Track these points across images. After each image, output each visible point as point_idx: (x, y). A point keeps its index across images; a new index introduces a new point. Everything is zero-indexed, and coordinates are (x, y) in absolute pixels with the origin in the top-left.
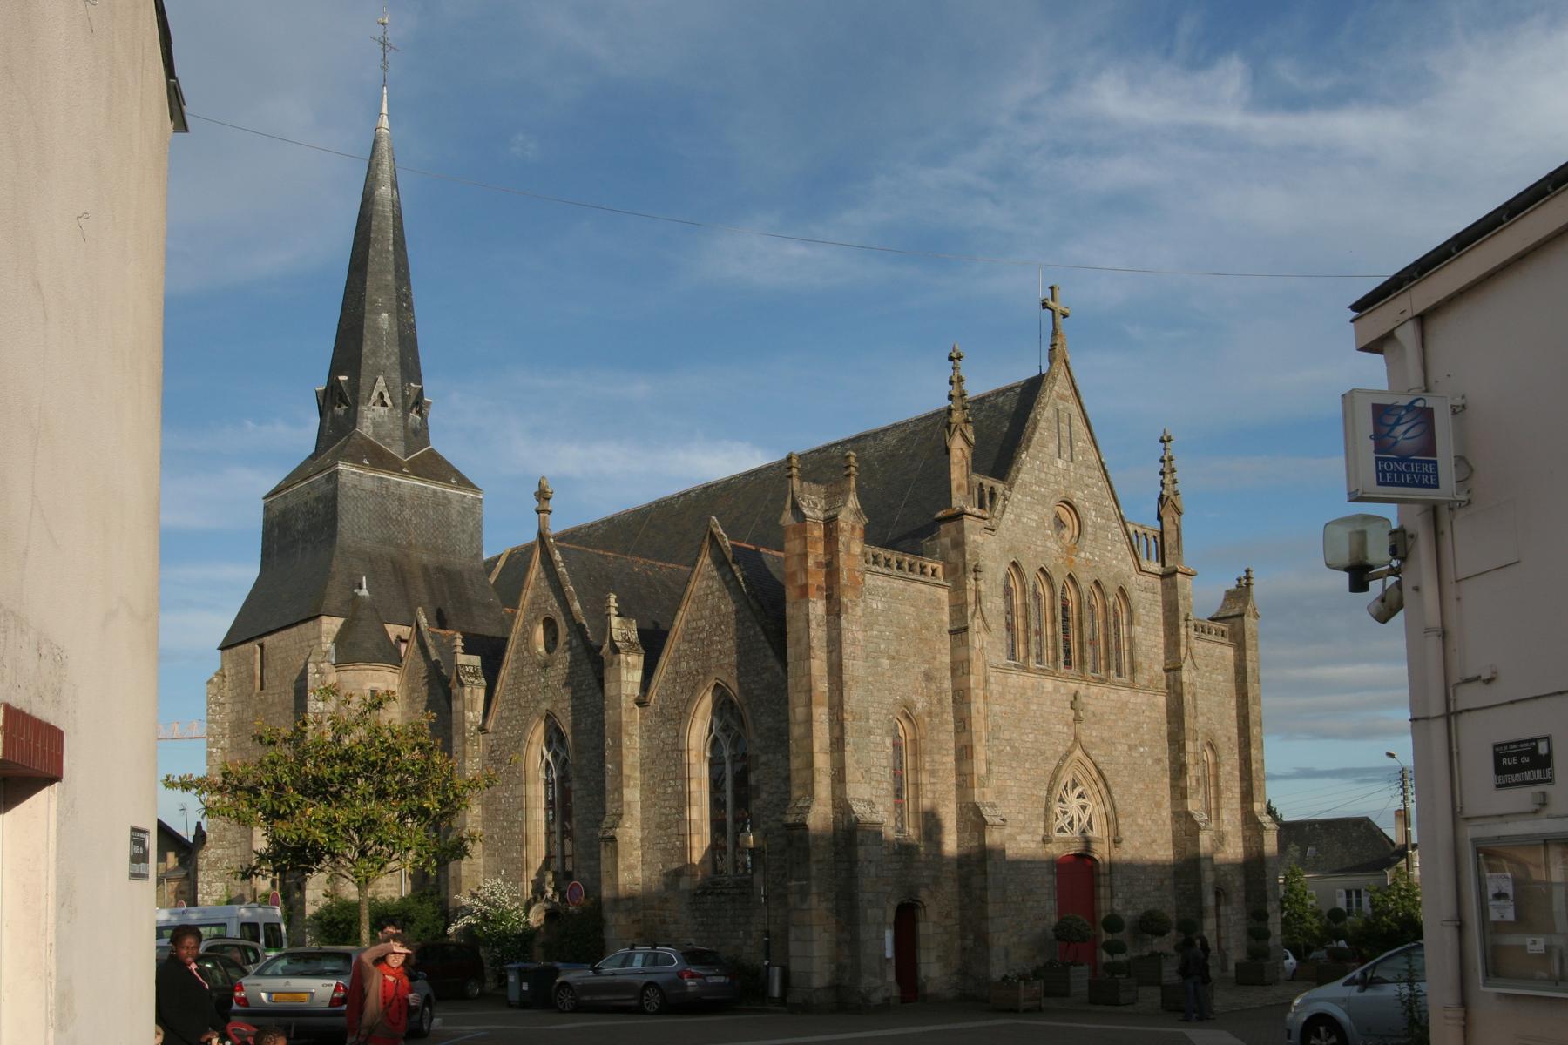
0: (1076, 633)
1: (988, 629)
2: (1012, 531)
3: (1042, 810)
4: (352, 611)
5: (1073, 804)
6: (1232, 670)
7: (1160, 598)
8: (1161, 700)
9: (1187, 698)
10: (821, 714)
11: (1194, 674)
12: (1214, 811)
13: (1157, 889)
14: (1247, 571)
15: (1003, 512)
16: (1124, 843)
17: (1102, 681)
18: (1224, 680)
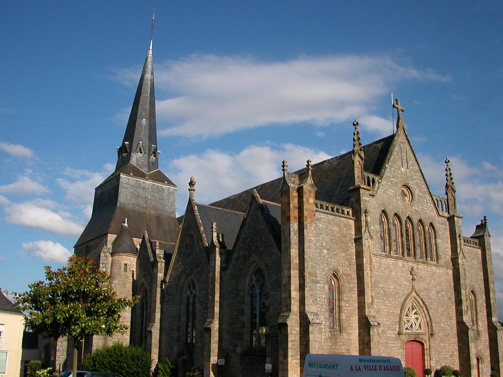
0: (411, 239)
1: (371, 238)
2: (381, 197)
3: (398, 320)
4: (121, 233)
5: (413, 317)
6: (480, 259)
7: (448, 227)
8: (450, 272)
9: (461, 271)
10: (295, 273)
11: (464, 260)
12: (475, 321)
13: (451, 356)
14: (485, 217)
15: (378, 188)
16: (436, 335)
17: (423, 263)
18: (477, 263)
